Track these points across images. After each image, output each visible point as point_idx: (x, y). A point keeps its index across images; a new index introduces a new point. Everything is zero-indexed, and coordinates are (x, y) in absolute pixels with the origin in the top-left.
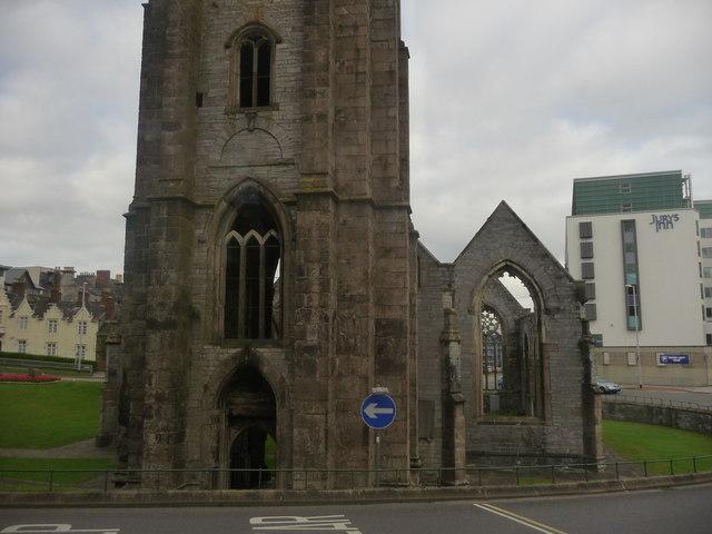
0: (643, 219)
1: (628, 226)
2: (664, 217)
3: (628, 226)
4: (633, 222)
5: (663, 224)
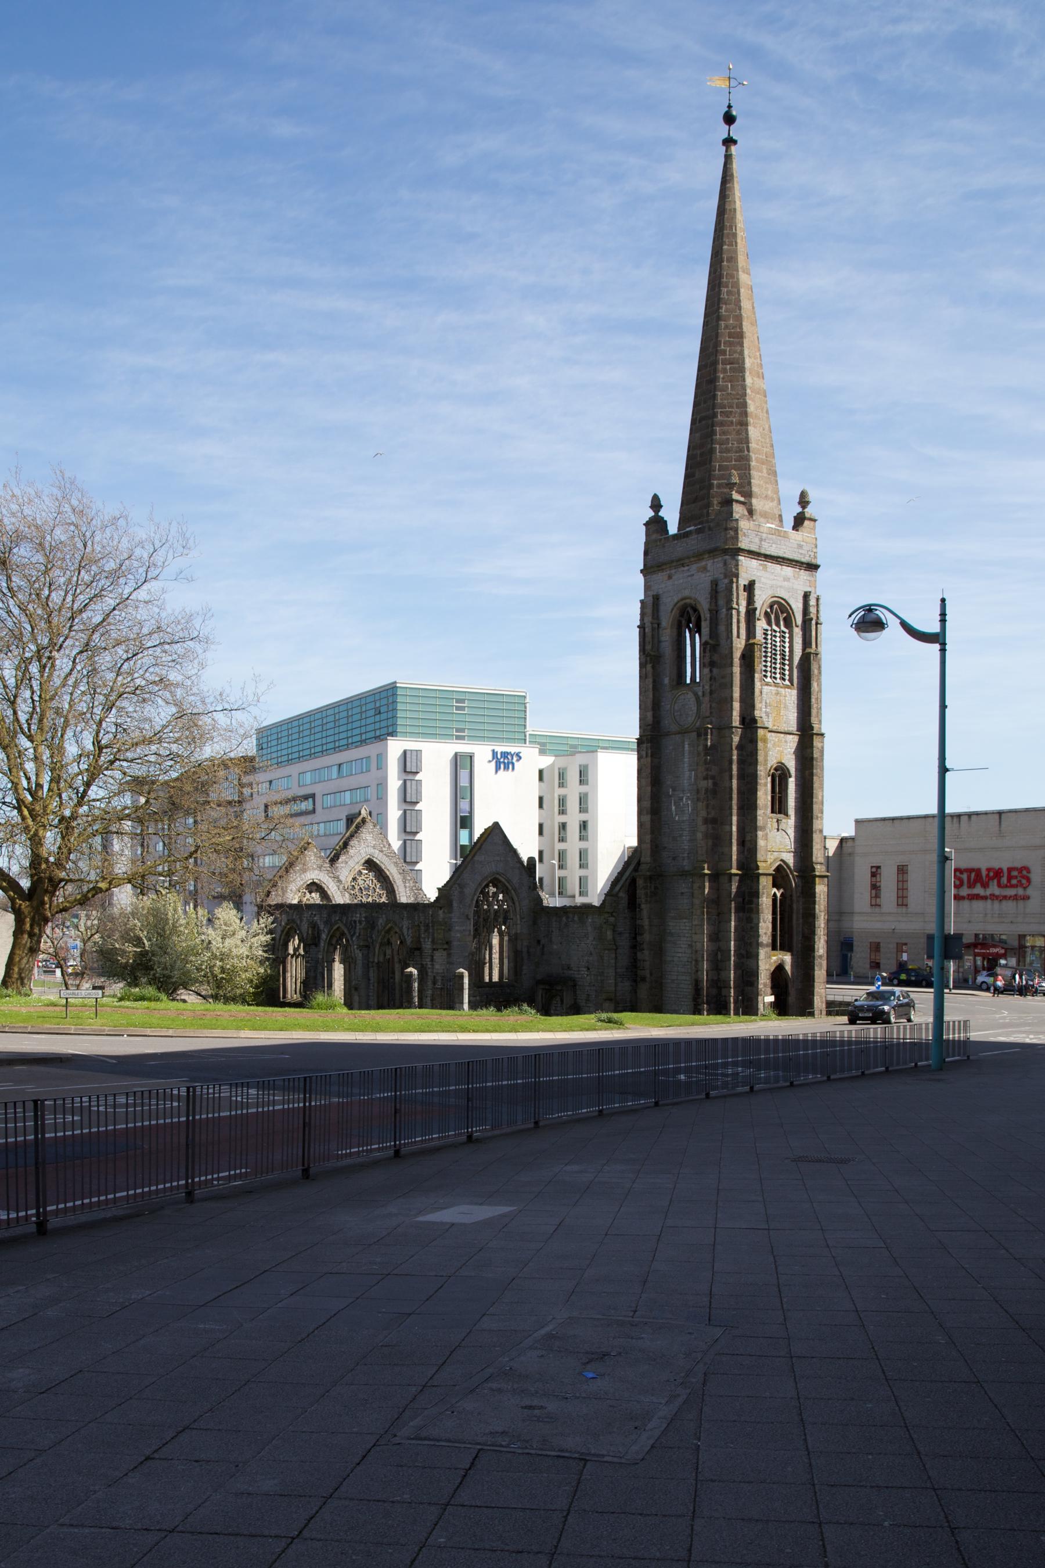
0: (482, 753)
1: (462, 764)
2: (505, 755)
3: (462, 764)
4: (471, 757)
5: (504, 762)
